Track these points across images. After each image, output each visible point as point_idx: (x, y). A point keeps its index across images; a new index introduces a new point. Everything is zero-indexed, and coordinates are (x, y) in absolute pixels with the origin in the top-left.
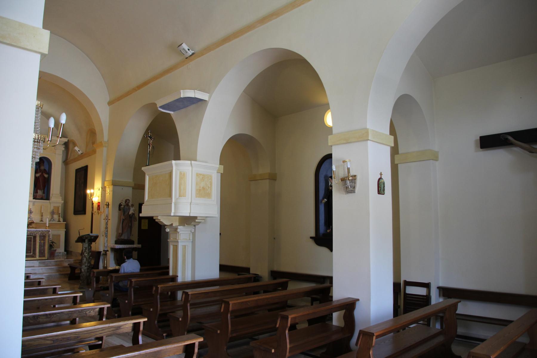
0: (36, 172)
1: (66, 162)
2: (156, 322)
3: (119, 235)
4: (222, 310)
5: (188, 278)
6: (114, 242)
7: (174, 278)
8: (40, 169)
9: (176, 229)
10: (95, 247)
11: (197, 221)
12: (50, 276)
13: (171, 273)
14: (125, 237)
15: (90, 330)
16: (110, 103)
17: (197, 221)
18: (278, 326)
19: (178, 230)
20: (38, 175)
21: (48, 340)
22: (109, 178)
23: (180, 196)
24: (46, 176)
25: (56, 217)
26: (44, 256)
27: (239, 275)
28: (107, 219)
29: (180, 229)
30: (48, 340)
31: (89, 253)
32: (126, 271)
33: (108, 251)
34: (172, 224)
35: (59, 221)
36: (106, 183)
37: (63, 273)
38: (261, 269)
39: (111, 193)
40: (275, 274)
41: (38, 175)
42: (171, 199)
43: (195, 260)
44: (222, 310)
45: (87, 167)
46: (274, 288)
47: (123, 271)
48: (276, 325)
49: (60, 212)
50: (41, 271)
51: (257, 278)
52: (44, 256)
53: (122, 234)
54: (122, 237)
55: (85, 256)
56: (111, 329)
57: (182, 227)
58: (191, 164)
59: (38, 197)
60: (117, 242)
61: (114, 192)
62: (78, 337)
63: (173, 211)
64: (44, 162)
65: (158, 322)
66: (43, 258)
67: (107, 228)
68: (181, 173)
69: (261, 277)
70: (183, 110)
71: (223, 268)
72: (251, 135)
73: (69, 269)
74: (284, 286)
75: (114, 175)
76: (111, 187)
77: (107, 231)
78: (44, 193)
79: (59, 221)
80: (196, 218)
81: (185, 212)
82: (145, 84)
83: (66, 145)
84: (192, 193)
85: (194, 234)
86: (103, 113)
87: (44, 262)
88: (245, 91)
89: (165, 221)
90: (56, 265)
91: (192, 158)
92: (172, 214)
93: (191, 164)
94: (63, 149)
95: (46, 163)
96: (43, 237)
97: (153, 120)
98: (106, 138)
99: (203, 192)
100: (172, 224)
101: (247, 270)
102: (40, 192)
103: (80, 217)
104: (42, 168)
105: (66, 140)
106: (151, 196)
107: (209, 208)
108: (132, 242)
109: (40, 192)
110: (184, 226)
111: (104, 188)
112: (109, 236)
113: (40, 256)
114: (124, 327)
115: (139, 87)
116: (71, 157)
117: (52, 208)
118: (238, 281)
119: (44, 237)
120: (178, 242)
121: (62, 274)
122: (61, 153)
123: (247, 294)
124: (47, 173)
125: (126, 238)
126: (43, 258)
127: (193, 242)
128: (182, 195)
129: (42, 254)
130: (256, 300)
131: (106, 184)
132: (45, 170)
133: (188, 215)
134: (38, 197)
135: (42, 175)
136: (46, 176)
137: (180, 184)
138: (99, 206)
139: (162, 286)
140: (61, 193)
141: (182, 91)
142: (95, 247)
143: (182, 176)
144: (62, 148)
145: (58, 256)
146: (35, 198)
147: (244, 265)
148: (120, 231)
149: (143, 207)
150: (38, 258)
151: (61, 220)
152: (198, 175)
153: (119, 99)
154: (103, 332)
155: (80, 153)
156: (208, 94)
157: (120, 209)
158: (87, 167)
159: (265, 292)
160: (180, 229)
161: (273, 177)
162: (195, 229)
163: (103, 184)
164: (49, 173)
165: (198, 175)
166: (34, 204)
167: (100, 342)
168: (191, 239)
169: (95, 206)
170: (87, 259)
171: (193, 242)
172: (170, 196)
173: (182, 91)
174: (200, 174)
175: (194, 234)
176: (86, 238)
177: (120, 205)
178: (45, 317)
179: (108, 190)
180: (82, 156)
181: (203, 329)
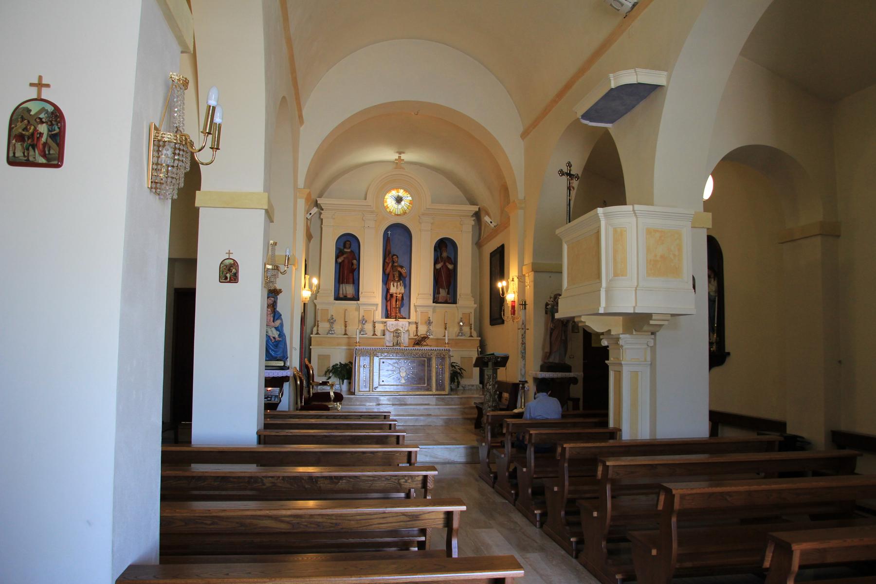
0: (436, 263)
1: (479, 244)
2: (563, 513)
3: (547, 356)
4: (660, 507)
5: (644, 434)
6: (539, 368)
7: (614, 434)
8: (442, 258)
9: (617, 339)
10: (503, 375)
11: (652, 322)
12: (449, 419)
13: (611, 424)
14: (555, 359)
15: (328, 515)
16: (524, 135)
17: (652, 322)
18: (767, 564)
19: (621, 342)
20: (439, 266)
21: (282, 521)
22: (528, 260)
23: (616, 275)
24: (450, 267)
25: (466, 329)
26: (444, 390)
27: (758, 434)
28: (524, 328)
29: (626, 339)
30: (282, 521)
31: (494, 385)
32: (532, 415)
33: (526, 382)
34: (609, 331)
35: (471, 336)
36: (524, 268)
37: (469, 416)
38: (811, 426)
39: (532, 284)
40: (839, 438)
41: (439, 266)
42: (600, 282)
43: (661, 398)
44: (660, 507)
45: (503, 247)
46: (845, 466)
47: (528, 417)
48: (763, 560)
49: (472, 322)
50: (437, 412)
51: (794, 443)
52: (444, 390)
53: (550, 353)
54: (551, 360)
55: (488, 390)
56: (403, 518)
57: (627, 336)
58: (634, 210)
59: (440, 300)
60: (543, 369)
61: (536, 284)
62: (336, 524)
63: (603, 303)
64: (446, 247)
65: (567, 513)
66: (443, 393)
67: (523, 343)
68: (615, 231)
69: (809, 443)
70: (627, 117)
71: (717, 419)
72: (775, 146)
73: (476, 411)
74: (845, 466)
75: (536, 253)
76: (532, 274)
77: (525, 349)
78: (448, 293)
79: (471, 336)
80: (649, 316)
81: (627, 304)
82: (568, 86)
83: (477, 216)
84: (168, 136)
85: (653, 349)
86: (513, 152)
87: (443, 399)
88: (744, 52)
89: (596, 325)
90: (461, 404)
91: (648, 200)
92: (601, 311)
93: (634, 210)
94: (473, 223)
95: (449, 246)
96: (442, 357)
97: (592, 152)
98: (521, 196)
99: (661, 265)
100: (609, 331)
101: (780, 426)
102: (443, 293)
103: (498, 328)
104: (445, 255)
105: (475, 208)
106: (571, 281)
107: (682, 296)
108: (568, 369)
109: (443, 293)
110: (632, 334)
111: (521, 278)
112: (527, 355)
113: (437, 390)
114: (427, 516)
115: (560, 95)
116: (484, 234)
117: (460, 316)
118: (769, 446)
119: (443, 359)
120: (621, 364)
121: (468, 419)
122: (470, 229)
123: (769, 476)
124: (451, 263)
125: (557, 361)
126: (443, 393)
127: (653, 365)
128: (619, 272)
129: (440, 387)
130: (749, 493)
131: (525, 270)
132: (449, 258)
133: (631, 311)
134: (440, 300)
135: (445, 266)
136: (450, 267)
137: (615, 251)
138: (513, 307)
139: (572, 445)
140: (472, 292)
141: (611, 75)
142: (503, 375)
143: (619, 236)
144: (471, 222)
145: (471, 390)
146: (435, 301)
147: (775, 416)
148: (547, 350)
149: (561, 301)
150: (434, 392)
151: (475, 334)
152: (650, 232)
153: (535, 124)
154: (381, 521)
155: (492, 225)
156: (665, 73)
157: (546, 313)
158: (503, 247)
159: (816, 474)
160: (626, 339)
161: (831, 232)
162: (655, 339)
163: (520, 270)
164: (455, 264)
165: (650, 232)
166: (434, 311)
167: (423, 539)
168: (649, 359)
169: (510, 305)
170: (491, 395)
171: (653, 365)
172: (599, 276)
173: (611, 75)
174: (656, 231)
175: (653, 349)
176: (489, 360)
177: (547, 305)
178: (327, 482)
179: (529, 280)
180: (497, 231)
181: (627, 540)
